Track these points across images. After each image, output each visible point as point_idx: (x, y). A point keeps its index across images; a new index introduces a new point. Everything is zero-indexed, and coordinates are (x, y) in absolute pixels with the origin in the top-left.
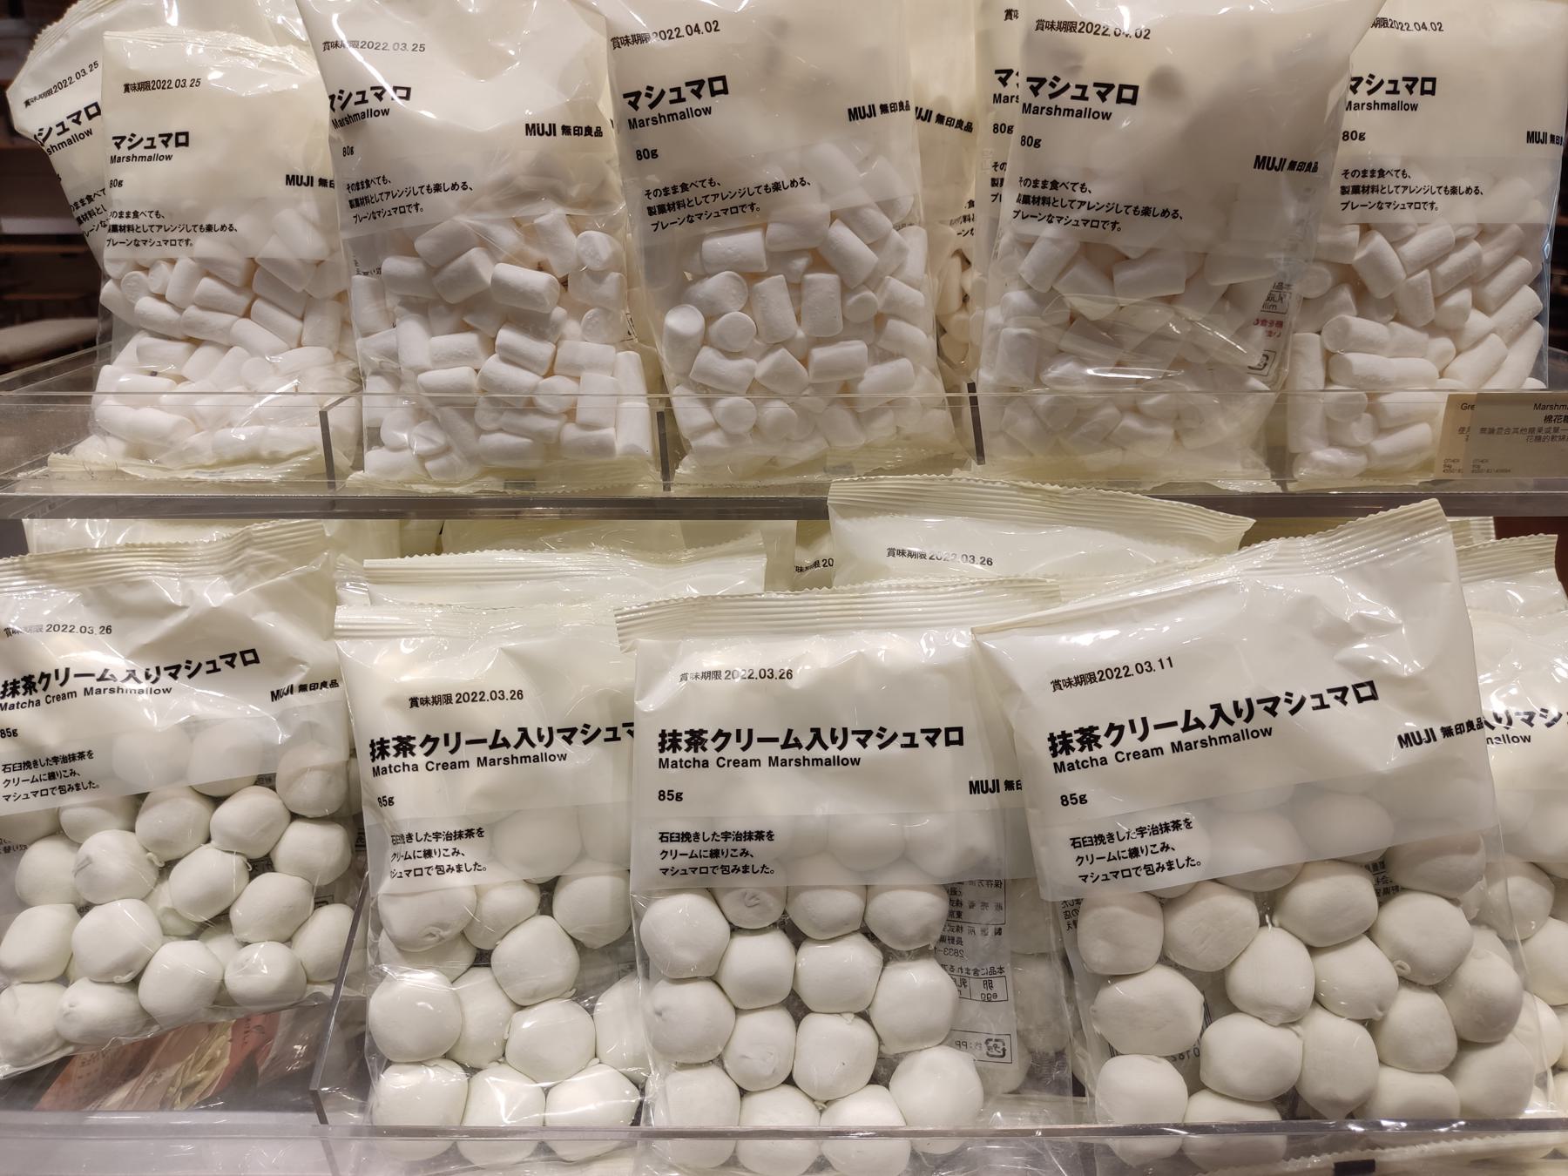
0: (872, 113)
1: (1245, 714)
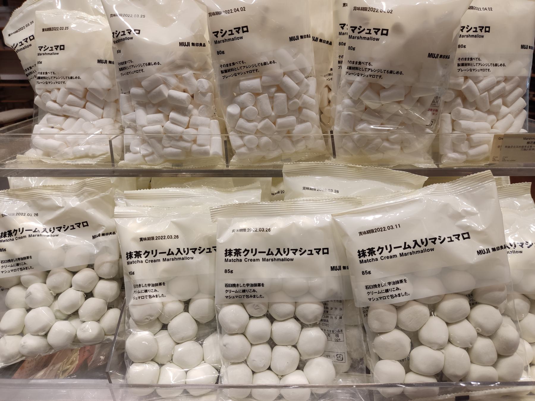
1: (425, 243)
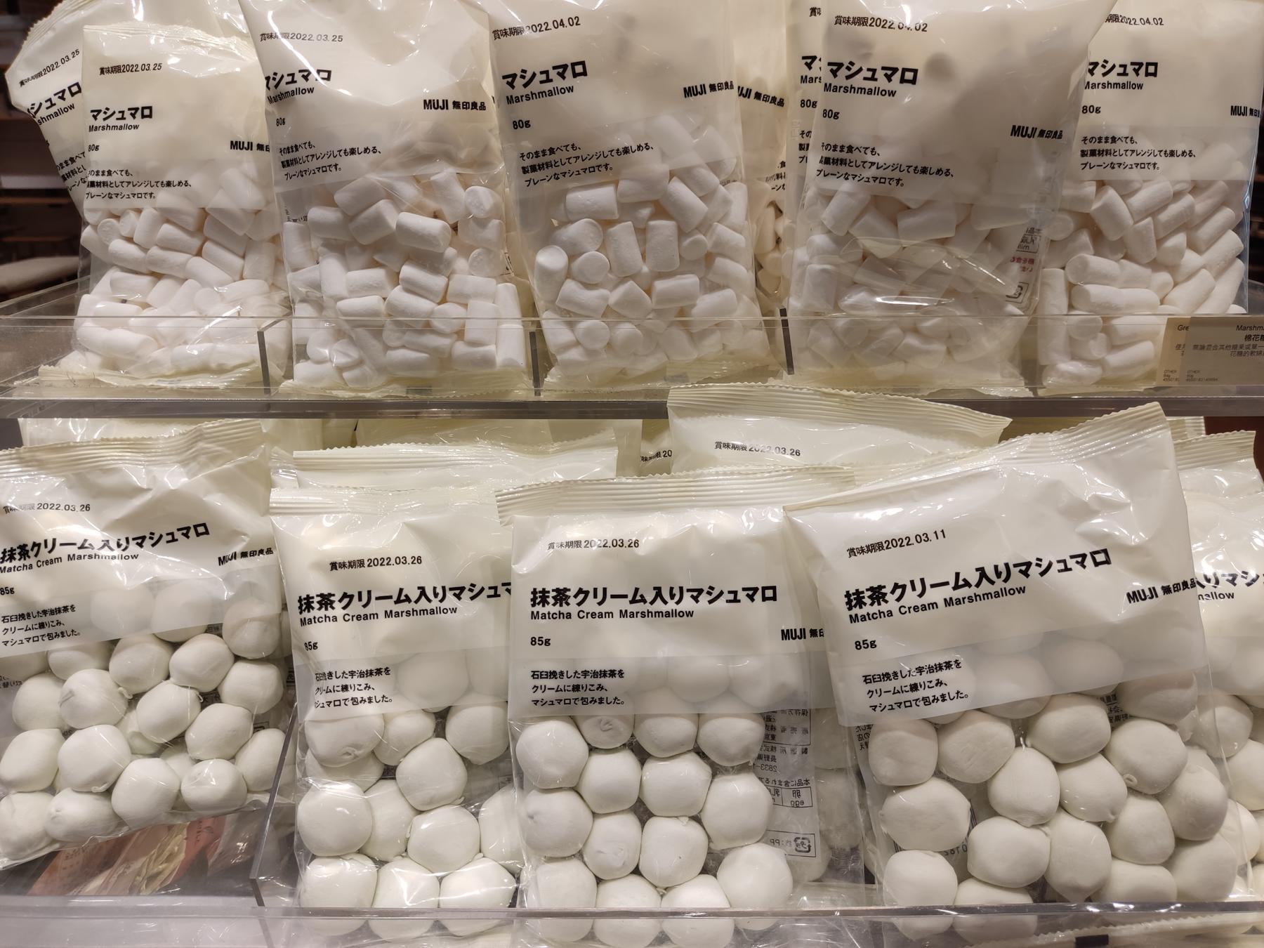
0: (703, 91)
1: (1004, 576)
